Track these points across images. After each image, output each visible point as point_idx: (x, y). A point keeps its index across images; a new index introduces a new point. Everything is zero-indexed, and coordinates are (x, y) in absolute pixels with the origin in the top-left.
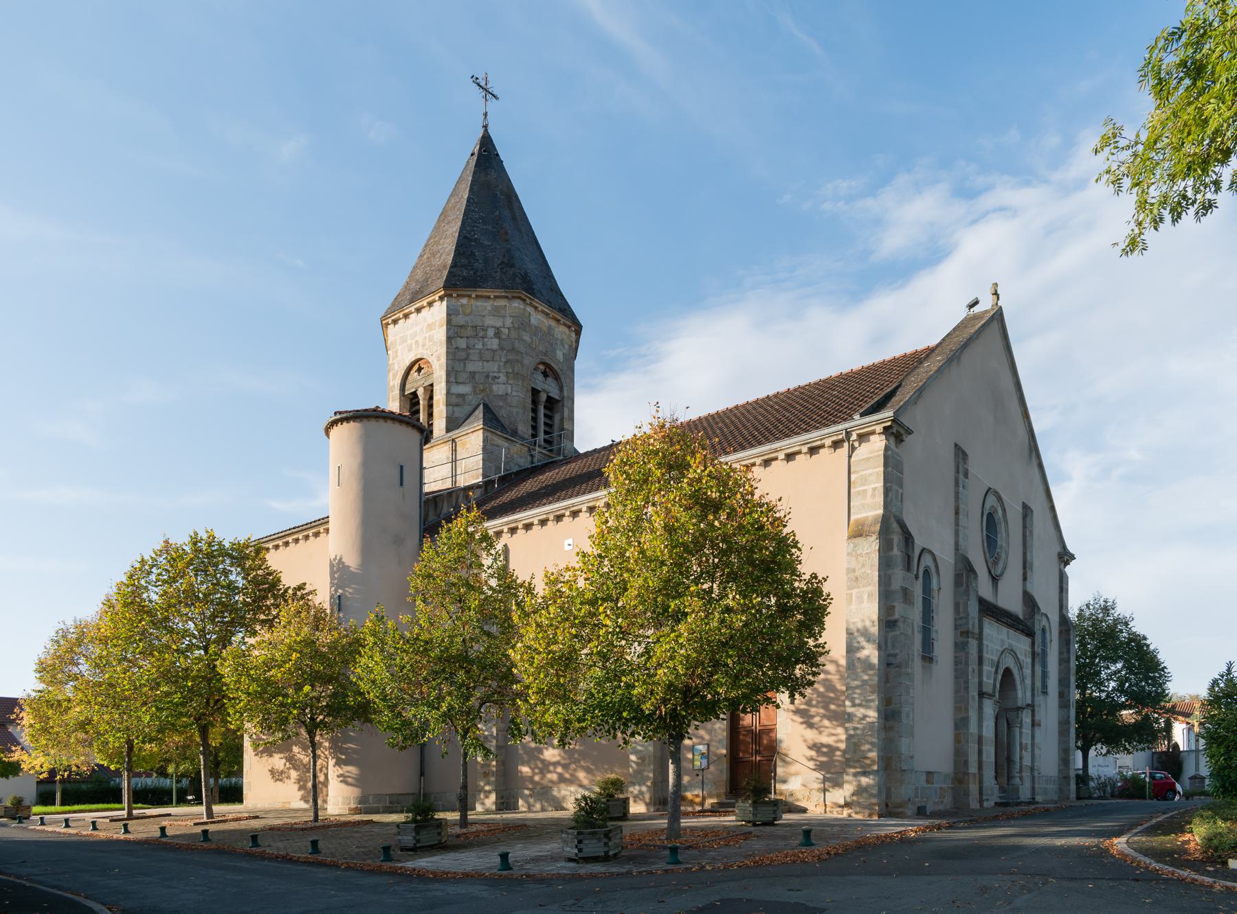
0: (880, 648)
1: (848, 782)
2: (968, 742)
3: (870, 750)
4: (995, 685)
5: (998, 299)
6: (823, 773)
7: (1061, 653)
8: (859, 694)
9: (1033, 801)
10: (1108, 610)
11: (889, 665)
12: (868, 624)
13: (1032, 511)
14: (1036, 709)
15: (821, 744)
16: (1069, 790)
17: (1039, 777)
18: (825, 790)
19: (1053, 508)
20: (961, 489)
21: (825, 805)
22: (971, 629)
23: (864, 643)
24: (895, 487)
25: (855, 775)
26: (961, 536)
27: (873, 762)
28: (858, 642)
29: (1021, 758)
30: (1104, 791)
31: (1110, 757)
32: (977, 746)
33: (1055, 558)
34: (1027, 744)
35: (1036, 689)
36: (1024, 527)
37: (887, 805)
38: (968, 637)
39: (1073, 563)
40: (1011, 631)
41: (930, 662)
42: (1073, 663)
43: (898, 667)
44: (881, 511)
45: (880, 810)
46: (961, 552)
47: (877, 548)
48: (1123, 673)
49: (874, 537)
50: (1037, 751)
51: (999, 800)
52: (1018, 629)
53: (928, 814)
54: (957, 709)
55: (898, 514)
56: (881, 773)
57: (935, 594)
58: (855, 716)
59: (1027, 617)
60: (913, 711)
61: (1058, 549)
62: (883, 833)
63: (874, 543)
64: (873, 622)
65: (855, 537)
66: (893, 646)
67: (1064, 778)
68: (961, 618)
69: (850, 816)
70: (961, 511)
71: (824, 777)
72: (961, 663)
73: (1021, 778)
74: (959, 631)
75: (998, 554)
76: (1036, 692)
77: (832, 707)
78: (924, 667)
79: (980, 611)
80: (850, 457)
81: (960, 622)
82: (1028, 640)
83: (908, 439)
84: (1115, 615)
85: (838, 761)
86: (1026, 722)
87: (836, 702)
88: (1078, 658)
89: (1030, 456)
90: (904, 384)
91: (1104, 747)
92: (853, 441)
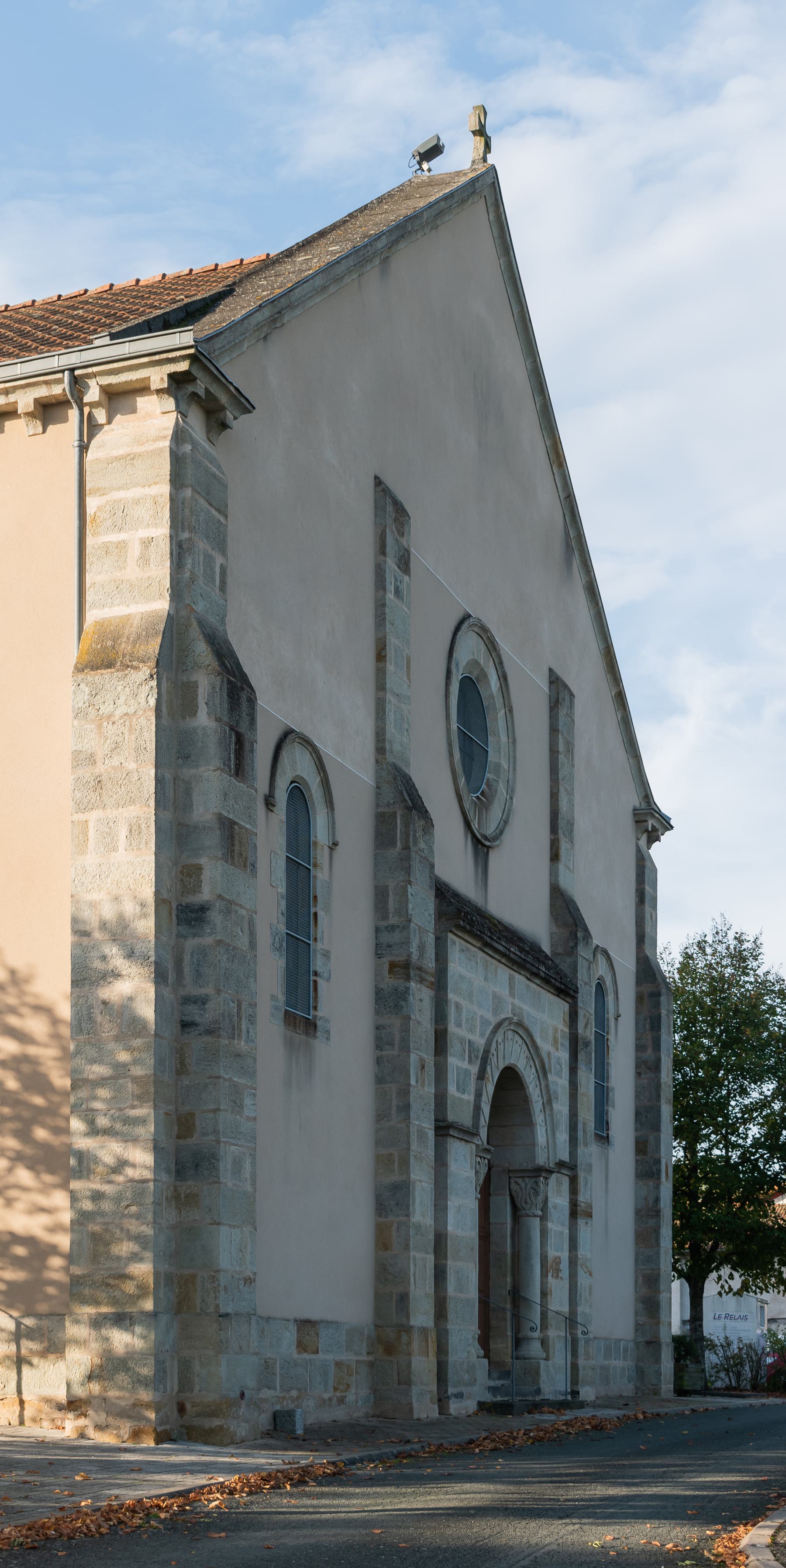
0: (160, 977)
1: (77, 1342)
2: (407, 1247)
3: (135, 1257)
4: (477, 1108)
5: (488, 147)
6: (15, 1314)
7: (640, 1048)
8: (104, 1100)
9: (572, 1401)
10: (744, 960)
11: (186, 1025)
12: (129, 908)
13: (572, 695)
14: (581, 1175)
15: (12, 1234)
16: (659, 1373)
17: (587, 1341)
18: (20, 1362)
19: (620, 699)
20: (390, 596)
21: (22, 1403)
22: (415, 957)
23: (119, 962)
24: (202, 545)
25: (97, 1323)
26: (391, 717)
27: (142, 1289)
28: (104, 958)
29: (544, 1294)
30: (739, 1375)
31: (751, 1300)
32: (431, 1257)
33: (628, 822)
34: (558, 1261)
35: (580, 1126)
36: (554, 730)
37: (182, 1409)
38: (408, 978)
39: (667, 837)
40: (520, 979)
41: (307, 1034)
42: (667, 1076)
43: (210, 1032)
44: (162, 605)
45: (161, 1421)
46: (390, 758)
47: (152, 702)
48: (777, 1106)
49: (145, 671)
50: (583, 1279)
51: (488, 1398)
52: (537, 975)
53: (300, 1432)
54: (382, 1162)
55: (212, 619)
56: (164, 1319)
57: (322, 855)
58: (96, 1160)
59: (560, 950)
60: (253, 1156)
61: (634, 800)
62: (129, 1496)
63: (145, 689)
64: (143, 905)
65: (94, 667)
66: (198, 974)
67: (649, 1343)
68: (391, 928)
69: (82, 1436)
70: (390, 653)
71: (18, 1324)
72: (391, 1044)
73: (544, 1342)
74: (386, 961)
75: (488, 785)
76: (580, 1134)
77: (41, 1134)
78: (289, 1044)
79: (440, 915)
80: (83, 448)
81: (386, 938)
82: (561, 1007)
83: (240, 424)
84: (760, 972)
85: (52, 1283)
86: (555, 1207)
87: (49, 1121)
88: (678, 1064)
89: (568, 563)
90: (238, 290)
91: (736, 1275)
92: (92, 405)
